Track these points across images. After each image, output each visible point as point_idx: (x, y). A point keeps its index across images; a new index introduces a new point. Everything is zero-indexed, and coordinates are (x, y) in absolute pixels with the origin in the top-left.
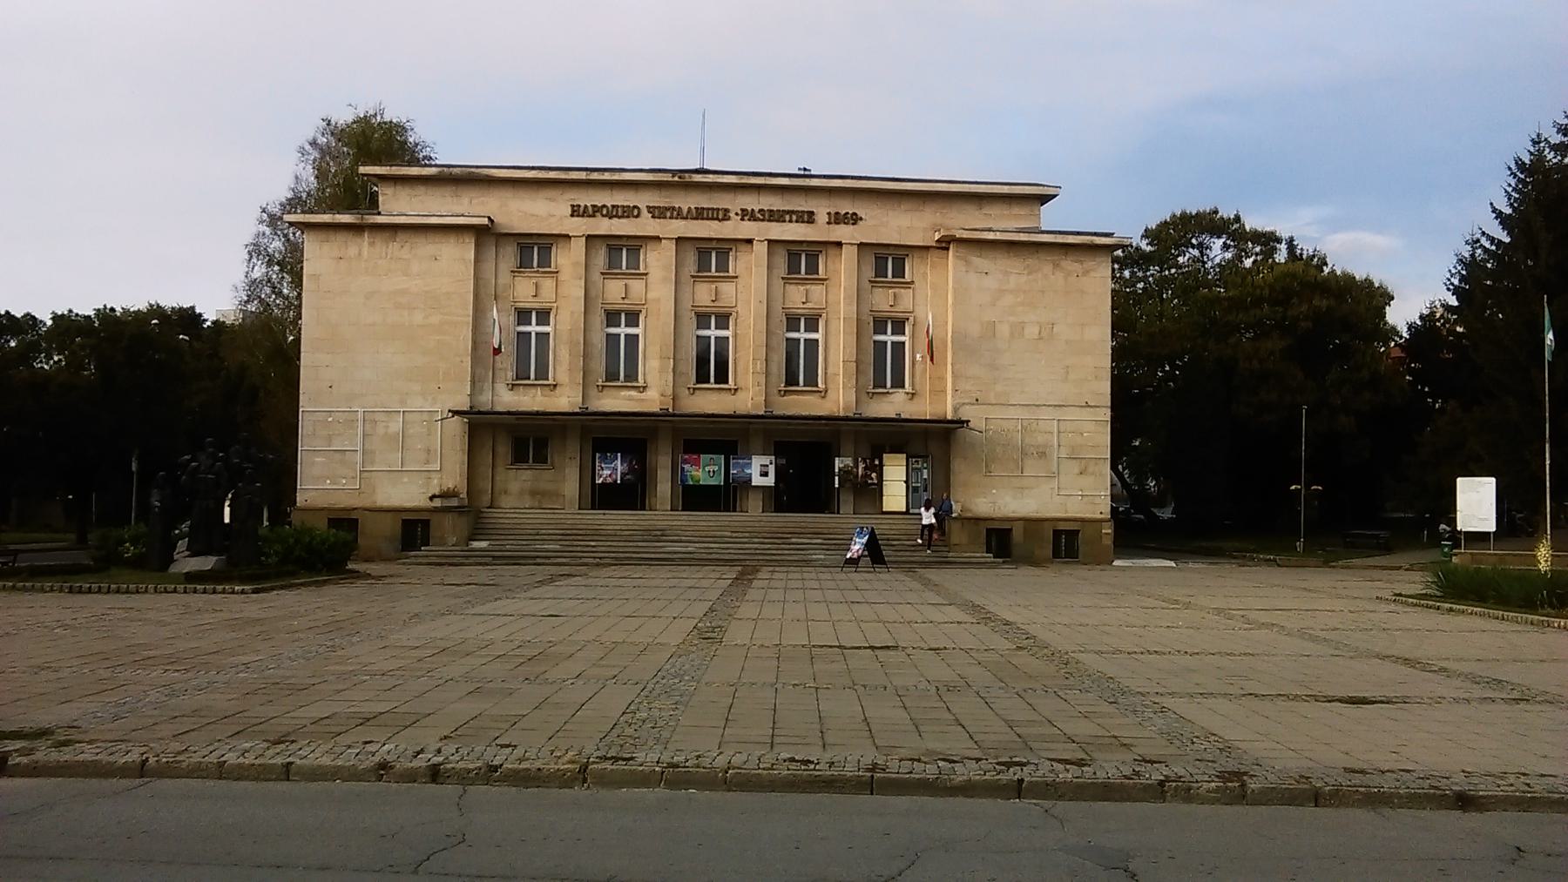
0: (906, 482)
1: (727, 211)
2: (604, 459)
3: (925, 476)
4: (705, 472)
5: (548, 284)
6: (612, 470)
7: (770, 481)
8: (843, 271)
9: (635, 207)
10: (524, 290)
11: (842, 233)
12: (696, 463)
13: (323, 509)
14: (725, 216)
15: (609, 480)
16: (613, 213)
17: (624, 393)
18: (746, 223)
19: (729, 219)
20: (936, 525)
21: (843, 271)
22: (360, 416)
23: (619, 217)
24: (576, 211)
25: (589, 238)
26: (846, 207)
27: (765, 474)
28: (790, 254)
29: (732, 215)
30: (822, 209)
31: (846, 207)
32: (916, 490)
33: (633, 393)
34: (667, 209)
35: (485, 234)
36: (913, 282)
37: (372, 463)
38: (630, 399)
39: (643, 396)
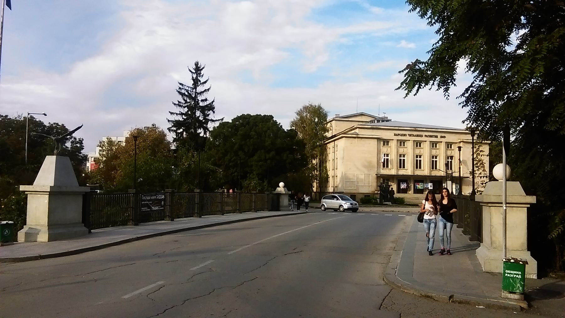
0: (455, 188)
1: (422, 135)
2: (402, 184)
3: (459, 187)
4: (420, 186)
5: (389, 149)
6: (403, 186)
7: (432, 188)
8: (442, 147)
9: (406, 134)
10: (384, 150)
11: (443, 140)
12: (419, 185)
13: (349, 193)
14: (422, 136)
15: (404, 188)
16: (402, 135)
17: (403, 170)
18: (426, 138)
19: (423, 137)
20: (275, 192)
21: (442, 147)
22: (356, 175)
23: (403, 136)
24: (395, 135)
25: (397, 140)
26: (443, 135)
27: (431, 187)
28: (383, 142)
29: (423, 136)
30: (439, 135)
31: (443, 135)
32: (457, 190)
33: (405, 171)
34: (433, 136)
35: (379, 139)
36: (454, 149)
37: (358, 184)
38: (405, 172)
39: (407, 171)
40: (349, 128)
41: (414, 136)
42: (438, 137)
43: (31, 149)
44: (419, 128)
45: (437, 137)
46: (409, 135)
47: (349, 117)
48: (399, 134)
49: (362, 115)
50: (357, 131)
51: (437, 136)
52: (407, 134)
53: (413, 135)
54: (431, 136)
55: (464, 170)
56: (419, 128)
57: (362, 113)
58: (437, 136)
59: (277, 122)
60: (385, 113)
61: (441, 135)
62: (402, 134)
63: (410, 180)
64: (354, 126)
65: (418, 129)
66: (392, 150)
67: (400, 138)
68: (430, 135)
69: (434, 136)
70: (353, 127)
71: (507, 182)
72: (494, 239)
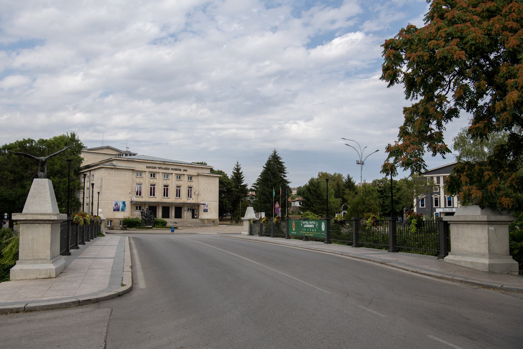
1: (169, 168)
5: (141, 179)
11: (185, 173)
17: (153, 198)
24: (147, 167)
26: (185, 169)
29: (170, 169)
30: (182, 169)
33: (155, 198)
40: (106, 160)
41: (163, 169)
42: (182, 170)
43: (464, 184)
44: (167, 162)
45: (181, 171)
46: (158, 167)
47: (96, 149)
48: (150, 167)
49: (108, 148)
50: (114, 163)
51: (181, 169)
52: (170, 168)
53: (161, 168)
54: (176, 170)
55: (272, 200)
56: (167, 162)
57: (109, 146)
58: (181, 169)
59: (80, 154)
60: (128, 148)
61: (184, 169)
62: (153, 167)
63: (184, 207)
64: (111, 158)
65: (167, 163)
66: (146, 181)
67: (151, 170)
68: (175, 169)
69: (178, 169)
70: (110, 159)
71: (441, 207)
72: (33, 278)
